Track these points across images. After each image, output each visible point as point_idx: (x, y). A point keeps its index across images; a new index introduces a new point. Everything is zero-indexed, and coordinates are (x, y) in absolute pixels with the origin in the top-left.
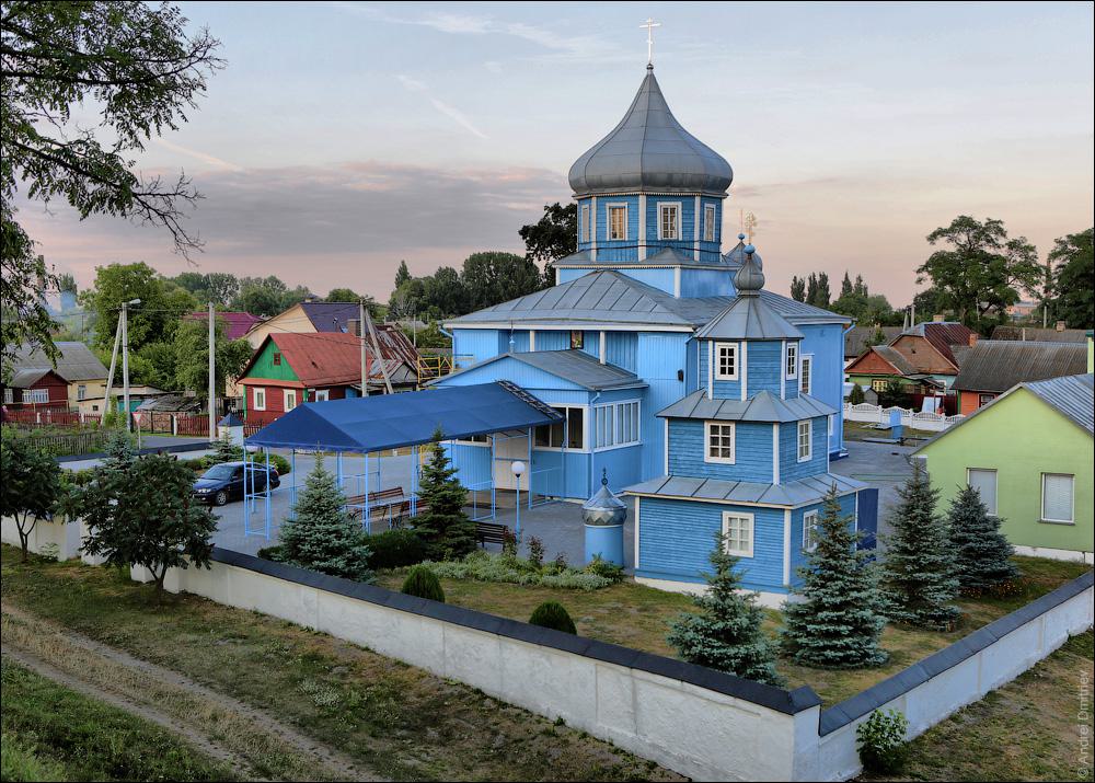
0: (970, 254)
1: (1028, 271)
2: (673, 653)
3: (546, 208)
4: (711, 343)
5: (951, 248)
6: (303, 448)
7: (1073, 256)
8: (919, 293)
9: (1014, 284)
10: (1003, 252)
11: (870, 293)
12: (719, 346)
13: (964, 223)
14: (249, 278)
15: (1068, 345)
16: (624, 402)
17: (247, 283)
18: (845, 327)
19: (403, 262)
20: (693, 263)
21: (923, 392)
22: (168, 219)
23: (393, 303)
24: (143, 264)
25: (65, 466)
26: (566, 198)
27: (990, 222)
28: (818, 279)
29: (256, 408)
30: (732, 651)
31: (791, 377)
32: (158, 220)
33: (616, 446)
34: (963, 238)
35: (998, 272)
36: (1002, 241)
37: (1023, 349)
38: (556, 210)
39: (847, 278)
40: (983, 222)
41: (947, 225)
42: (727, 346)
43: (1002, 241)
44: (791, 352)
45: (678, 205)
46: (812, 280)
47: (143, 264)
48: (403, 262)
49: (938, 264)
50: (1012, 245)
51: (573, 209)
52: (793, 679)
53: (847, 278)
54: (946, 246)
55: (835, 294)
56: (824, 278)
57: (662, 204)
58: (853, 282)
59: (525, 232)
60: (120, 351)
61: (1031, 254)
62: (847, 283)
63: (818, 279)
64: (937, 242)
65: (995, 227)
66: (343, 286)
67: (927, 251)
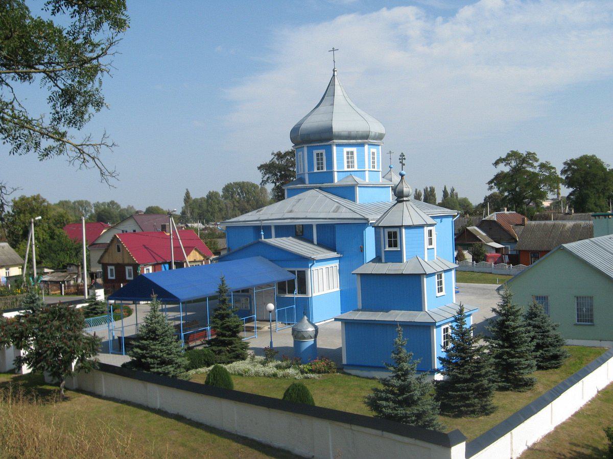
0: (517, 171)
1: (553, 181)
2: (367, 412)
3: (273, 154)
4: (382, 230)
5: (507, 169)
6: (144, 301)
7: (574, 171)
8: (487, 195)
9: (543, 188)
10: (537, 170)
11: (460, 196)
12: (387, 230)
13: (513, 155)
14: (98, 202)
15: (579, 222)
16: (329, 266)
17: (97, 206)
18: (454, 216)
19: (187, 190)
20: (365, 183)
21: (204, 262)
22: (96, 159)
23: (183, 213)
24: (38, 196)
25: (569, 342)
26: (288, 146)
27: (529, 153)
28: (429, 189)
29: (110, 277)
30: (408, 412)
31: (431, 247)
32: (91, 163)
33: (326, 291)
34: (513, 164)
35: (533, 182)
36: (536, 164)
37: (554, 225)
38: (279, 156)
39: (445, 188)
40: (525, 154)
41: (504, 156)
42: (392, 230)
43: (536, 164)
44: (430, 232)
45: (323, 151)
46: (425, 190)
47: (38, 196)
48: (187, 190)
49: (499, 179)
50: (543, 166)
51: (292, 153)
52: (445, 424)
53: (445, 188)
54: (505, 168)
55: (439, 198)
56: (432, 190)
57: (316, 151)
58: (449, 191)
59: (261, 168)
60: (31, 246)
61: (553, 170)
62: (445, 192)
63: (429, 189)
64: (498, 166)
65: (531, 156)
66: (154, 204)
67: (493, 172)
